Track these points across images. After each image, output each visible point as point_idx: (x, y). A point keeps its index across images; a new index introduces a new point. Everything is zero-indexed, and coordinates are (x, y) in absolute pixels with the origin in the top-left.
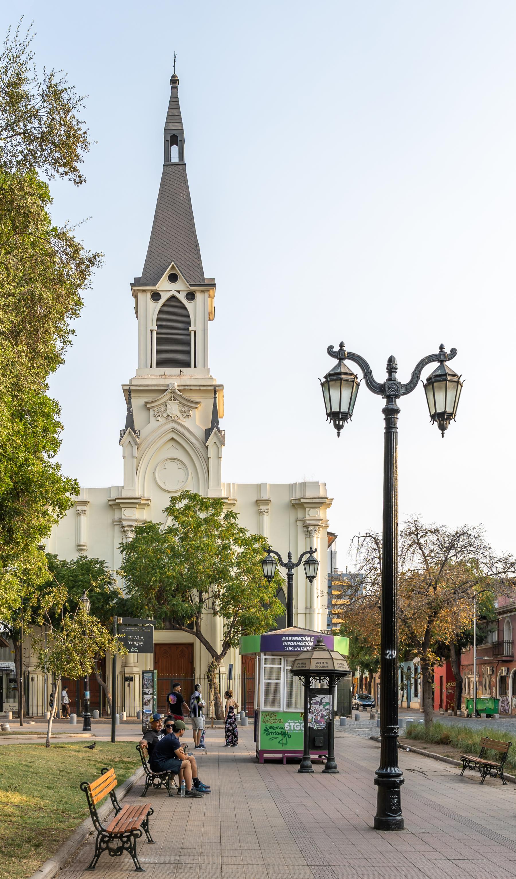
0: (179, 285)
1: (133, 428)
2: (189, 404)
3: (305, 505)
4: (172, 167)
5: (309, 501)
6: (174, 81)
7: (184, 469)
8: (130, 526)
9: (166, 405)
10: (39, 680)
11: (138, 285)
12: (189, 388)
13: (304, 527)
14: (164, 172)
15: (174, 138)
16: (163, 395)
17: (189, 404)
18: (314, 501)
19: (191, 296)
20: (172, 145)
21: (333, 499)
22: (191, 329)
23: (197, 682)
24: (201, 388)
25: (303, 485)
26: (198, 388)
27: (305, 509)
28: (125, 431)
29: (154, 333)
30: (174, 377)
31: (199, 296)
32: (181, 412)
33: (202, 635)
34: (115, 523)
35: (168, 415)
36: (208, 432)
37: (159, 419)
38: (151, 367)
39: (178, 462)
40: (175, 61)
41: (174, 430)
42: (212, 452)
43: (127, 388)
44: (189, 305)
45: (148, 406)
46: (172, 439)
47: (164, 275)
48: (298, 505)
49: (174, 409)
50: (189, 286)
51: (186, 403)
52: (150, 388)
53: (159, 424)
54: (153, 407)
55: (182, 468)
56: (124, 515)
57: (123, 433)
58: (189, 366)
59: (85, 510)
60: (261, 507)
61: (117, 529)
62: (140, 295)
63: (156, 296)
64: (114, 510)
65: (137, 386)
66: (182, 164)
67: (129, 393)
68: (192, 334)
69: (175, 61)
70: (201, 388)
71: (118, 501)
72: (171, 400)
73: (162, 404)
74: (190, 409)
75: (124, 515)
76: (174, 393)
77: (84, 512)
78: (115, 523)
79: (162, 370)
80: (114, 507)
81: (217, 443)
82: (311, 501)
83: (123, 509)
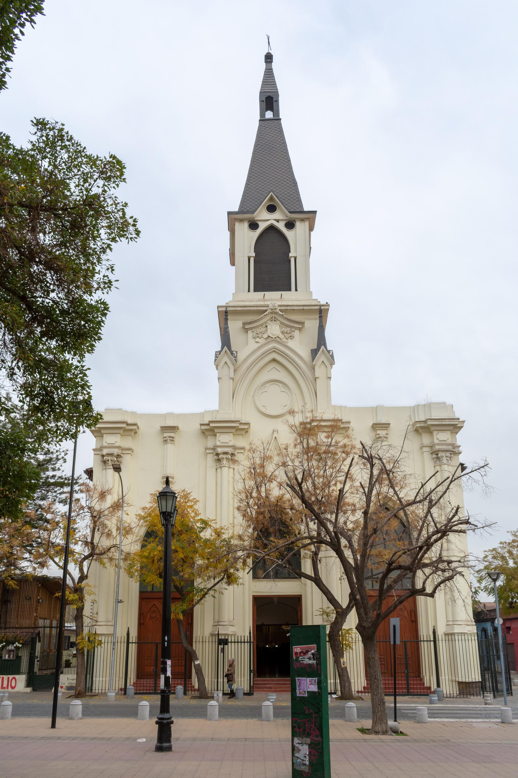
0: (277, 215)
1: (229, 348)
2: (292, 324)
3: (432, 428)
4: (268, 121)
5: (437, 423)
6: (269, 58)
7: (287, 391)
8: (226, 453)
9: (266, 326)
10: (119, 644)
11: (233, 218)
12: (292, 308)
13: (432, 453)
14: (260, 126)
15: (269, 101)
16: (263, 315)
17: (292, 324)
18: (443, 423)
19: (290, 225)
20: (267, 110)
21: (464, 422)
22: (290, 255)
23: (197, 647)
24: (305, 308)
25: (429, 406)
26: (301, 308)
27: (431, 433)
28: (220, 352)
29: (252, 260)
30: (273, 298)
31: (298, 225)
32: (283, 333)
33: (322, 581)
34: (207, 451)
35: (269, 336)
36: (314, 353)
37: (258, 340)
38: (249, 291)
39: (281, 385)
40: (269, 42)
41: (275, 350)
42: (319, 371)
43: (224, 309)
44: (289, 234)
45: (246, 327)
46: (274, 360)
47: (263, 204)
48: (424, 428)
49: (274, 329)
50: (289, 214)
51: (288, 323)
52: (249, 308)
53: (258, 345)
54: (252, 328)
55: (285, 391)
56: (219, 441)
57: (218, 354)
58: (289, 289)
59: (172, 437)
60: (378, 432)
61: (211, 458)
62: (237, 225)
63: (253, 226)
64: (206, 437)
65: (234, 307)
66: (277, 119)
67: (225, 315)
68: (292, 261)
69: (269, 42)
70: (305, 308)
71: (212, 425)
72: (272, 321)
73: (262, 325)
74: (293, 330)
75: (219, 441)
76: (276, 313)
77: (171, 439)
78: (207, 451)
79: (260, 294)
80: (207, 433)
81: (326, 362)
82: (440, 423)
83: (218, 435)
